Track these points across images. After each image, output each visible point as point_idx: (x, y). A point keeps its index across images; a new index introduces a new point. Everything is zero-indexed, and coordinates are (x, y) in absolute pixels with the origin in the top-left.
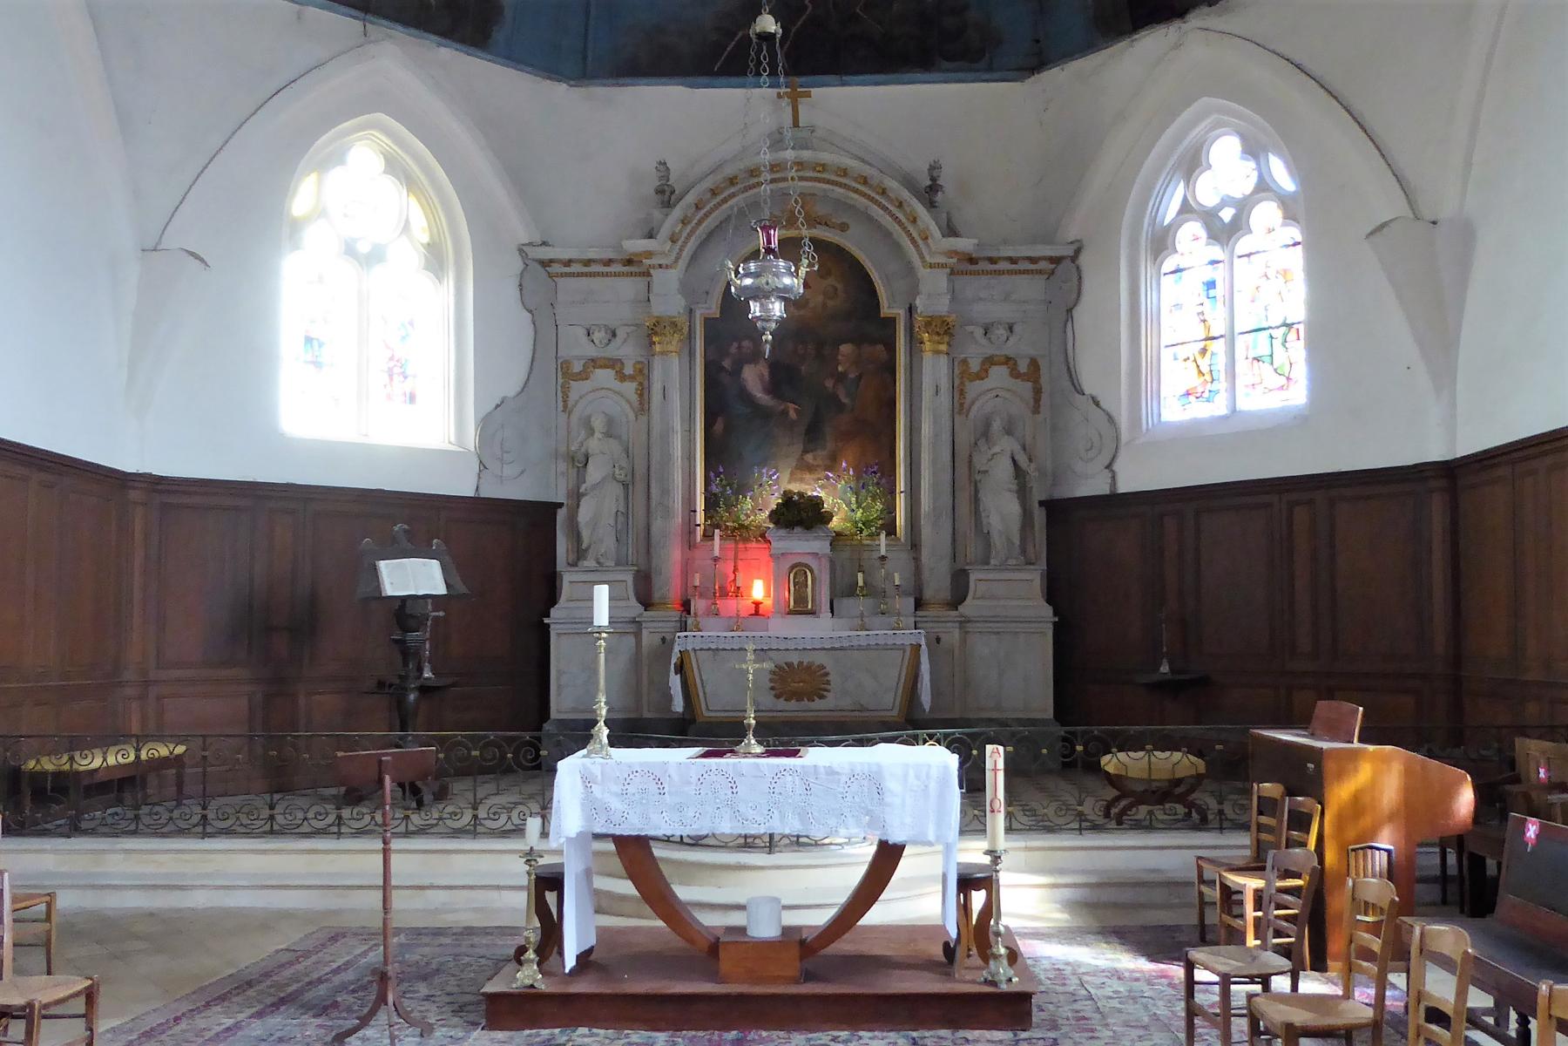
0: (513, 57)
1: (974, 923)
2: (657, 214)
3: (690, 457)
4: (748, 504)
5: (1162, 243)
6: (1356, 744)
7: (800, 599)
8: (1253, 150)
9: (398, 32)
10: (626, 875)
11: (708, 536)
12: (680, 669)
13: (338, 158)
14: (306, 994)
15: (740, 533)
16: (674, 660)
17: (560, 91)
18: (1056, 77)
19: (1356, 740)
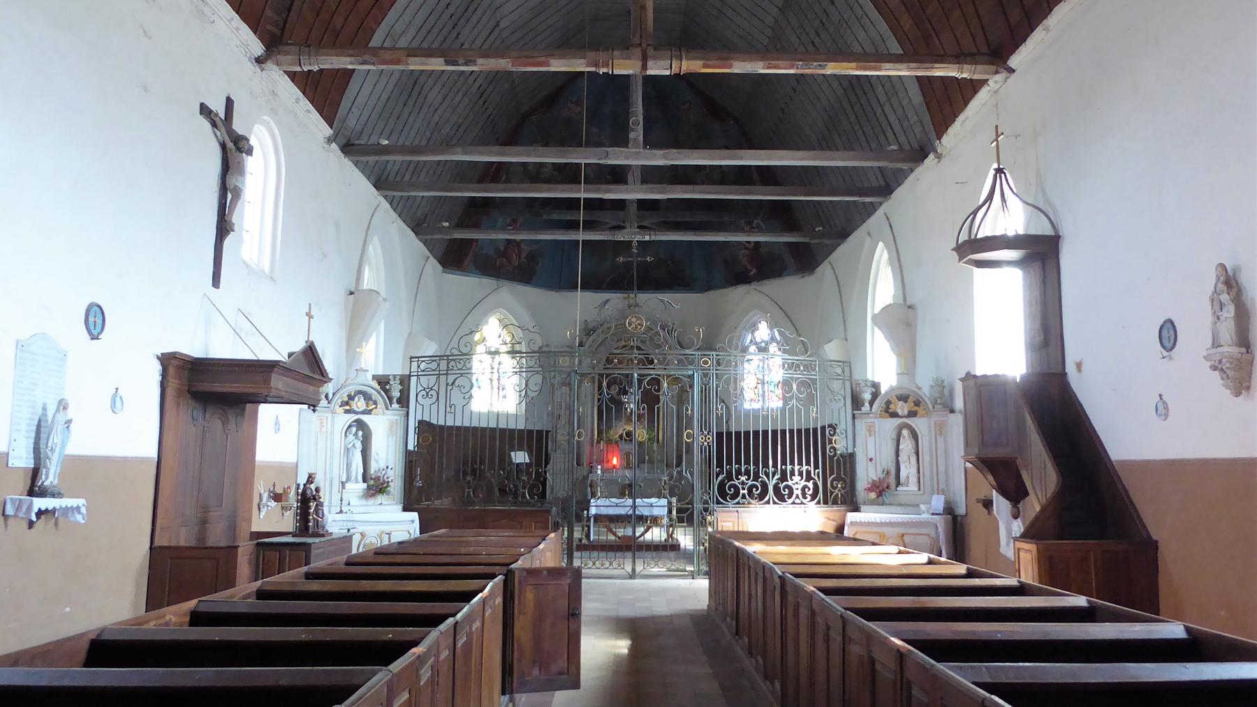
0: (538, 285)
1: (737, 544)
2: (585, 338)
3: (593, 417)
4: (612, 432)
5: (745, 350)
6: (642, 150)
7: (628, 464)
8: (771, 328)
9: (506, 282)
10: (196, 610)
11: (598, 442)
12: (591, 486)
13: (487, 322)
14: (1025, 472)
15: (609, 442)
16: (589, 483)
17: (553, 294)
18: (712, 294)
19: (637, 134)
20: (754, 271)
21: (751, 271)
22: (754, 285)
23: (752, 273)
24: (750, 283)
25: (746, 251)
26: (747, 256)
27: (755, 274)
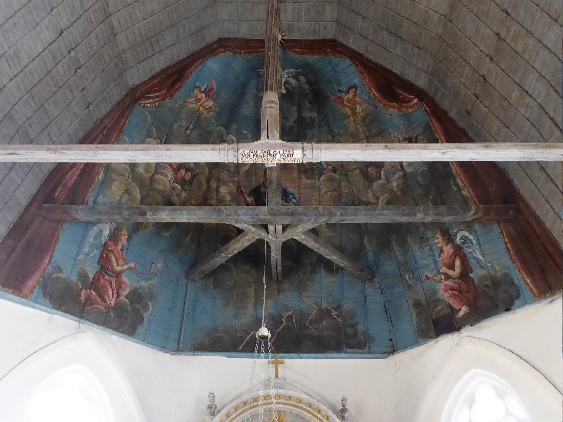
0: (146, 341)
20: (464, 310)
21: (460, 310)
22: (467, 331)
23: (461, 314)
24: (459, 330)
25: (450, 283)
26: (452, 289)
27: (465, 315)
